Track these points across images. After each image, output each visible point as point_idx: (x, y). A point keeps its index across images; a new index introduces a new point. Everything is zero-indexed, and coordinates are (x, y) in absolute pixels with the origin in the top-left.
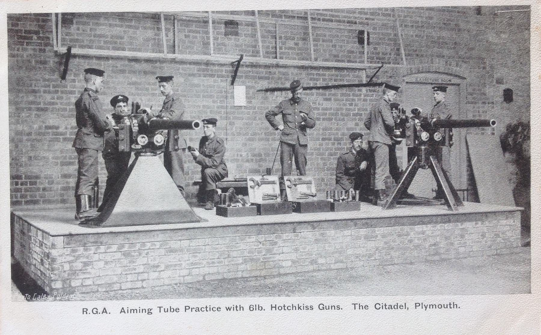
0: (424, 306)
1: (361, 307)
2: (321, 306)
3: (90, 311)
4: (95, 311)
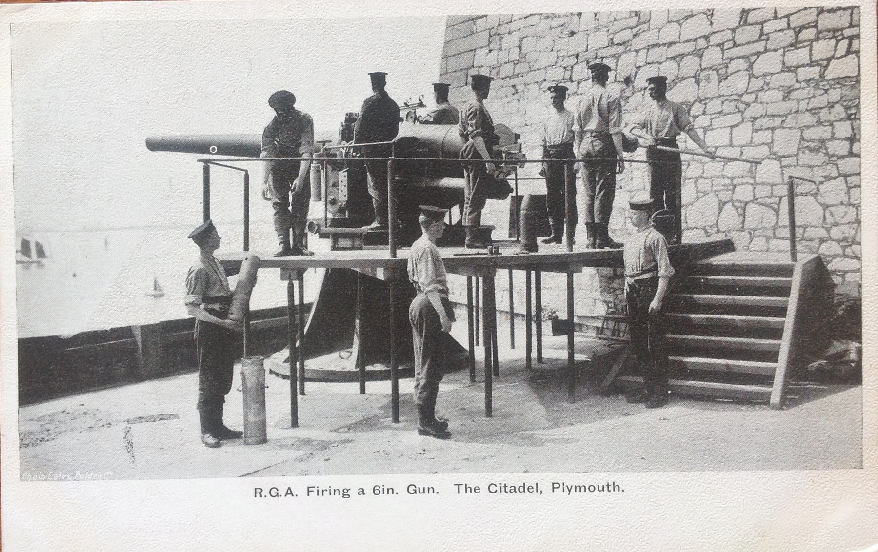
0: (566, 488)
1: (469, 490)
2: (411, 489)
3: (266, 492)
4: (273, 492)
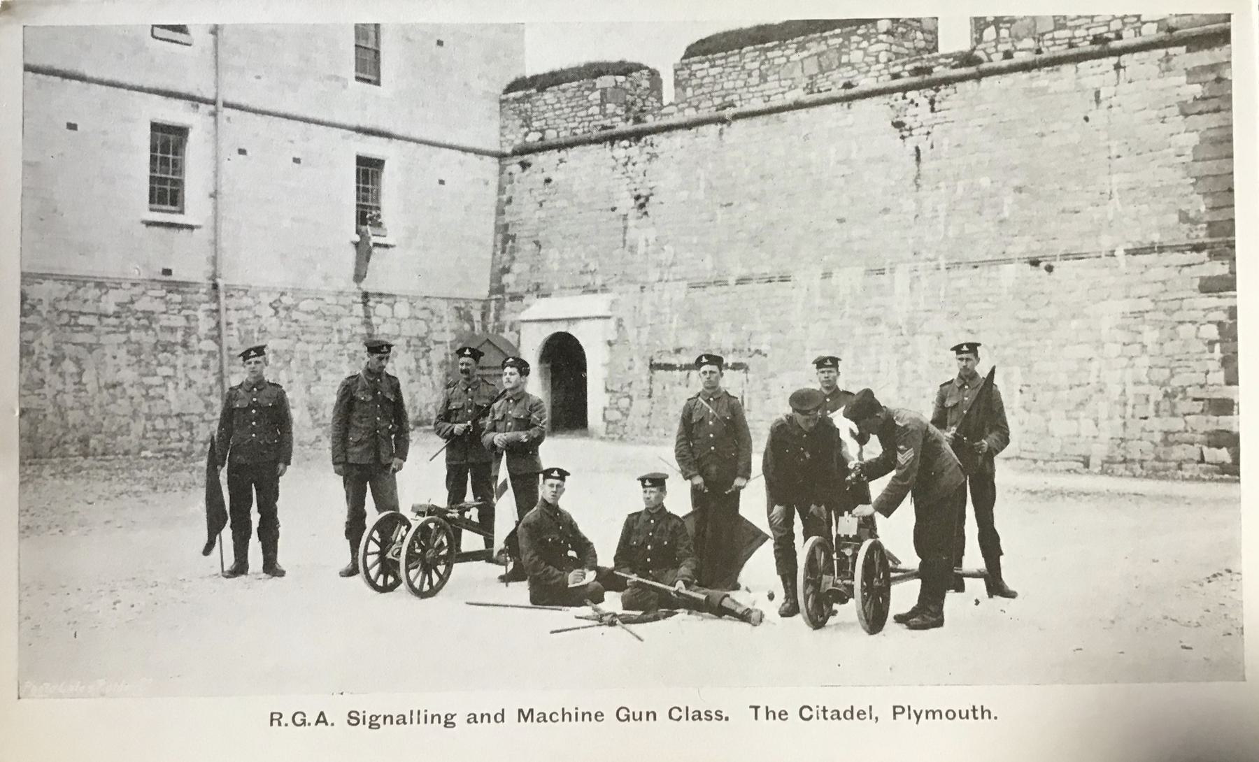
1: (771, 715)
2: (622, 714)
3: (286, 719)
4: (298, 719)
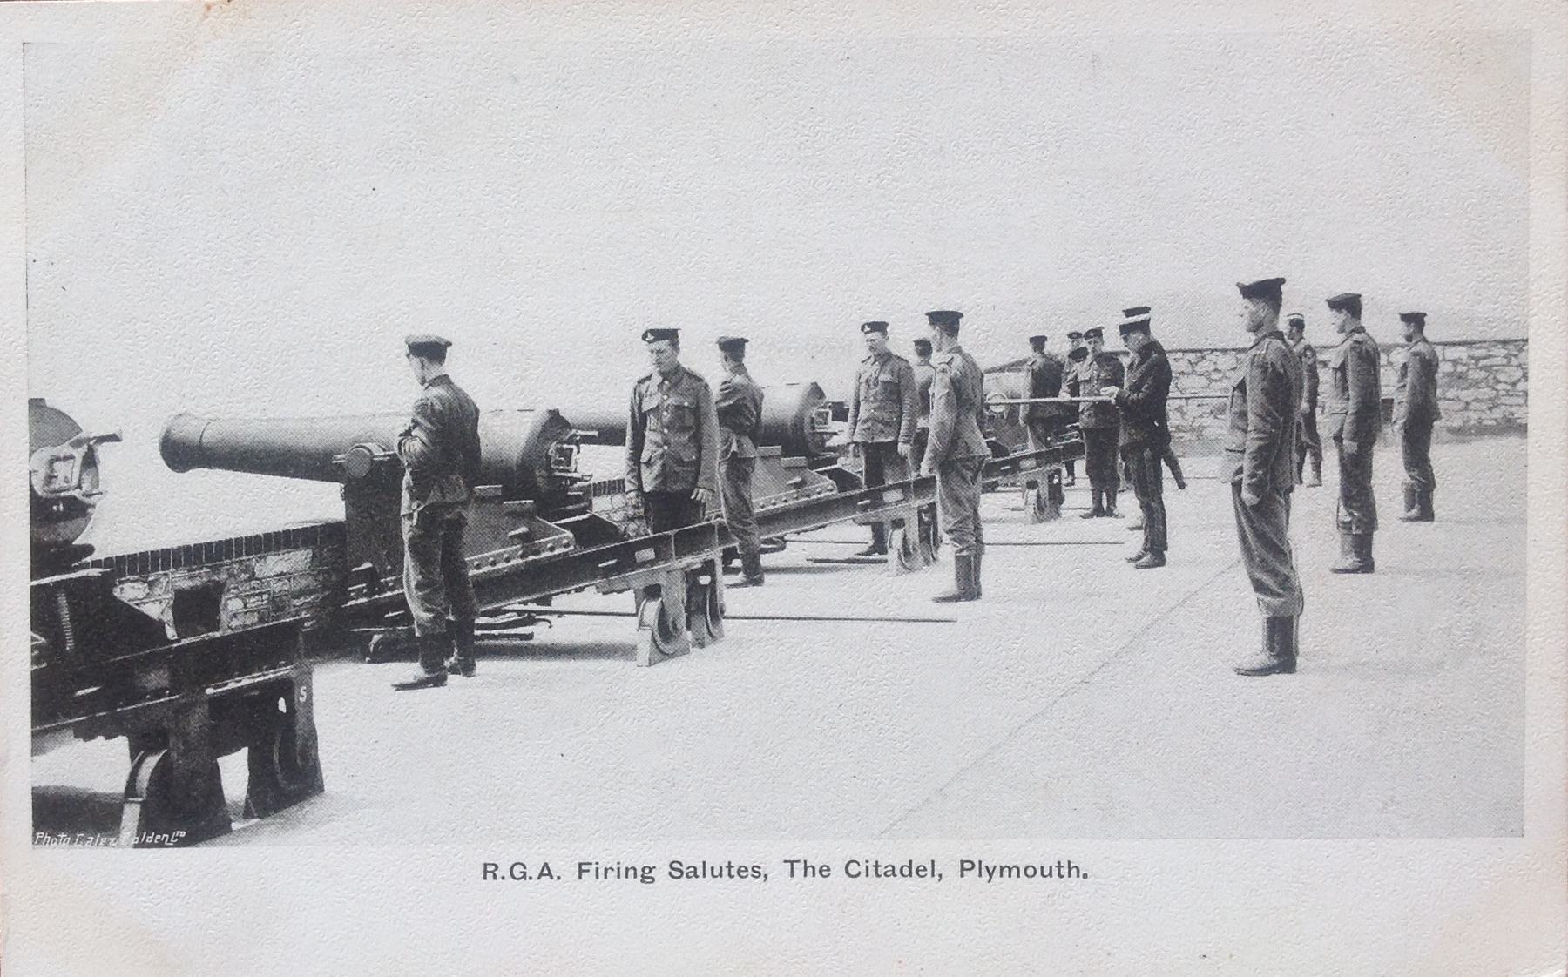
0: (984, 871)
1: (810, 870)
3: (503, 871)
4: (518, 870)
